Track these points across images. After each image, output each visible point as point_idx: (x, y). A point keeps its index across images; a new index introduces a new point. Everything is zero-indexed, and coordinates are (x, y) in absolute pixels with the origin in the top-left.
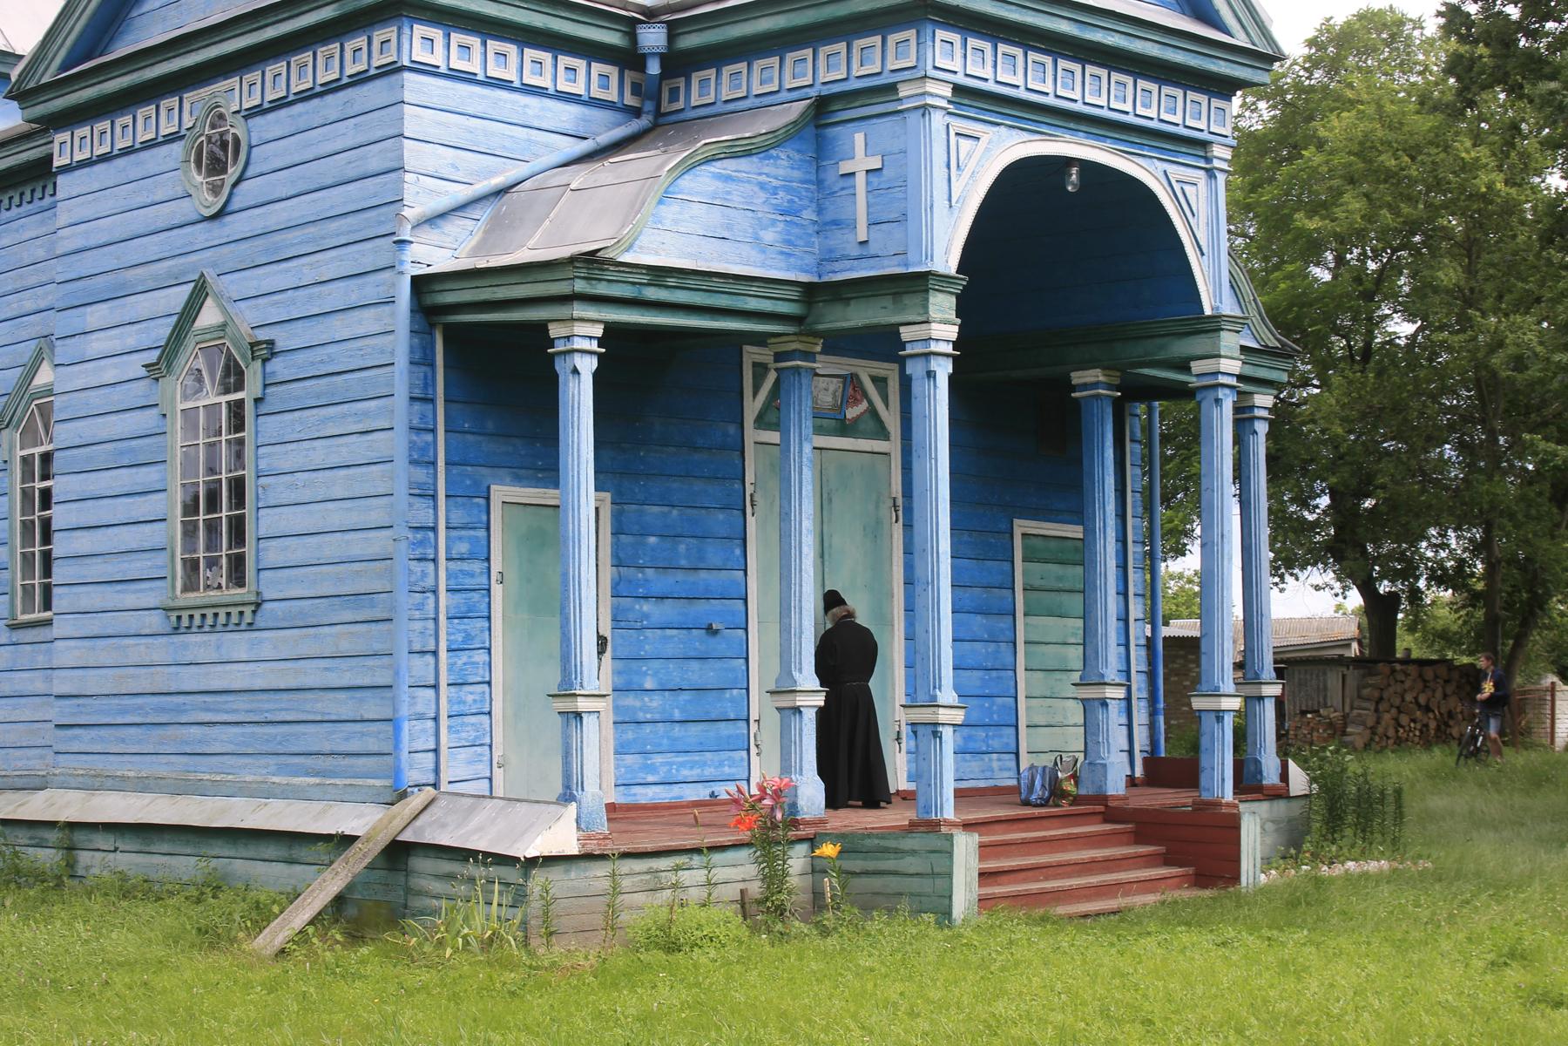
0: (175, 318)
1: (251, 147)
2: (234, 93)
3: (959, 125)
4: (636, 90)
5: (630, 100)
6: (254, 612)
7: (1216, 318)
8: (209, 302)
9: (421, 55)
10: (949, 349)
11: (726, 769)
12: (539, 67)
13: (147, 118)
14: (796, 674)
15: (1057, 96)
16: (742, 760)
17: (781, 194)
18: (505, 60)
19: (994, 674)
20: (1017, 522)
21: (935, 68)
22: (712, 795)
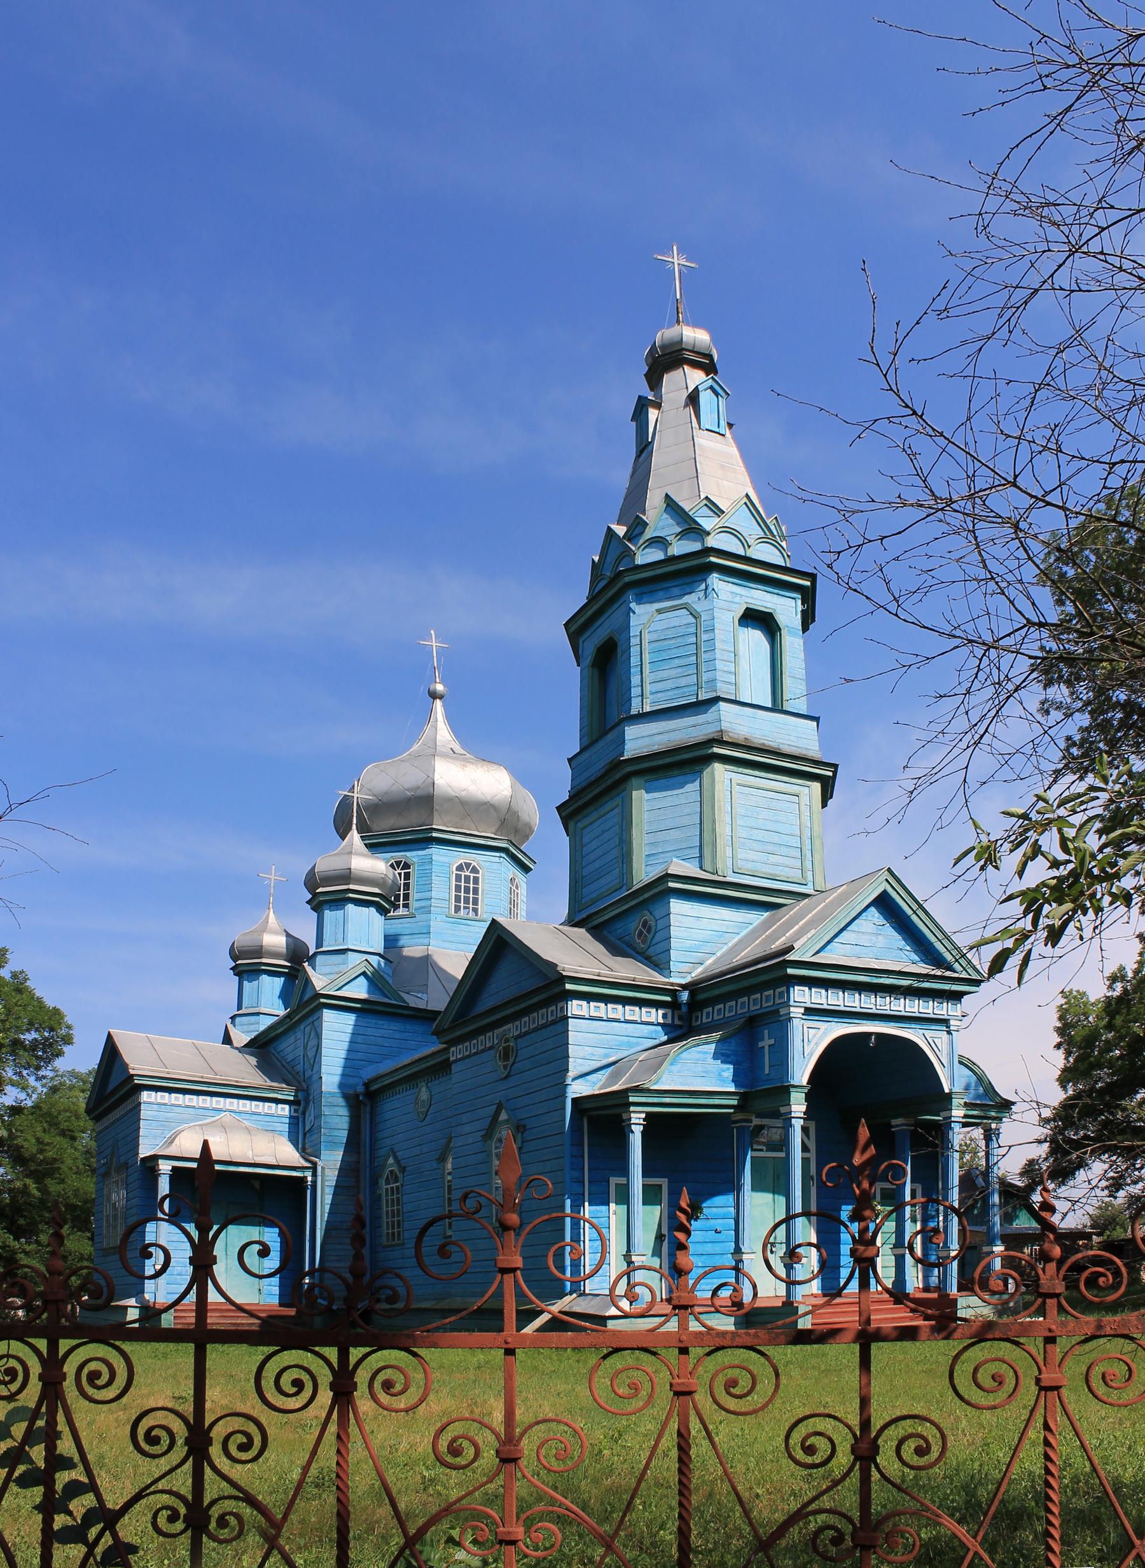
2: (512, 1029)
3: (811, 1024)
4: (680, 1018)
5: (677, 1022)
7: (950, 1094)
8: (503, 1111)
9: (577, 1012)
10: (802, 1115)
12: (633, 1012)
14: (741, 1246)
18: (616, 1011)
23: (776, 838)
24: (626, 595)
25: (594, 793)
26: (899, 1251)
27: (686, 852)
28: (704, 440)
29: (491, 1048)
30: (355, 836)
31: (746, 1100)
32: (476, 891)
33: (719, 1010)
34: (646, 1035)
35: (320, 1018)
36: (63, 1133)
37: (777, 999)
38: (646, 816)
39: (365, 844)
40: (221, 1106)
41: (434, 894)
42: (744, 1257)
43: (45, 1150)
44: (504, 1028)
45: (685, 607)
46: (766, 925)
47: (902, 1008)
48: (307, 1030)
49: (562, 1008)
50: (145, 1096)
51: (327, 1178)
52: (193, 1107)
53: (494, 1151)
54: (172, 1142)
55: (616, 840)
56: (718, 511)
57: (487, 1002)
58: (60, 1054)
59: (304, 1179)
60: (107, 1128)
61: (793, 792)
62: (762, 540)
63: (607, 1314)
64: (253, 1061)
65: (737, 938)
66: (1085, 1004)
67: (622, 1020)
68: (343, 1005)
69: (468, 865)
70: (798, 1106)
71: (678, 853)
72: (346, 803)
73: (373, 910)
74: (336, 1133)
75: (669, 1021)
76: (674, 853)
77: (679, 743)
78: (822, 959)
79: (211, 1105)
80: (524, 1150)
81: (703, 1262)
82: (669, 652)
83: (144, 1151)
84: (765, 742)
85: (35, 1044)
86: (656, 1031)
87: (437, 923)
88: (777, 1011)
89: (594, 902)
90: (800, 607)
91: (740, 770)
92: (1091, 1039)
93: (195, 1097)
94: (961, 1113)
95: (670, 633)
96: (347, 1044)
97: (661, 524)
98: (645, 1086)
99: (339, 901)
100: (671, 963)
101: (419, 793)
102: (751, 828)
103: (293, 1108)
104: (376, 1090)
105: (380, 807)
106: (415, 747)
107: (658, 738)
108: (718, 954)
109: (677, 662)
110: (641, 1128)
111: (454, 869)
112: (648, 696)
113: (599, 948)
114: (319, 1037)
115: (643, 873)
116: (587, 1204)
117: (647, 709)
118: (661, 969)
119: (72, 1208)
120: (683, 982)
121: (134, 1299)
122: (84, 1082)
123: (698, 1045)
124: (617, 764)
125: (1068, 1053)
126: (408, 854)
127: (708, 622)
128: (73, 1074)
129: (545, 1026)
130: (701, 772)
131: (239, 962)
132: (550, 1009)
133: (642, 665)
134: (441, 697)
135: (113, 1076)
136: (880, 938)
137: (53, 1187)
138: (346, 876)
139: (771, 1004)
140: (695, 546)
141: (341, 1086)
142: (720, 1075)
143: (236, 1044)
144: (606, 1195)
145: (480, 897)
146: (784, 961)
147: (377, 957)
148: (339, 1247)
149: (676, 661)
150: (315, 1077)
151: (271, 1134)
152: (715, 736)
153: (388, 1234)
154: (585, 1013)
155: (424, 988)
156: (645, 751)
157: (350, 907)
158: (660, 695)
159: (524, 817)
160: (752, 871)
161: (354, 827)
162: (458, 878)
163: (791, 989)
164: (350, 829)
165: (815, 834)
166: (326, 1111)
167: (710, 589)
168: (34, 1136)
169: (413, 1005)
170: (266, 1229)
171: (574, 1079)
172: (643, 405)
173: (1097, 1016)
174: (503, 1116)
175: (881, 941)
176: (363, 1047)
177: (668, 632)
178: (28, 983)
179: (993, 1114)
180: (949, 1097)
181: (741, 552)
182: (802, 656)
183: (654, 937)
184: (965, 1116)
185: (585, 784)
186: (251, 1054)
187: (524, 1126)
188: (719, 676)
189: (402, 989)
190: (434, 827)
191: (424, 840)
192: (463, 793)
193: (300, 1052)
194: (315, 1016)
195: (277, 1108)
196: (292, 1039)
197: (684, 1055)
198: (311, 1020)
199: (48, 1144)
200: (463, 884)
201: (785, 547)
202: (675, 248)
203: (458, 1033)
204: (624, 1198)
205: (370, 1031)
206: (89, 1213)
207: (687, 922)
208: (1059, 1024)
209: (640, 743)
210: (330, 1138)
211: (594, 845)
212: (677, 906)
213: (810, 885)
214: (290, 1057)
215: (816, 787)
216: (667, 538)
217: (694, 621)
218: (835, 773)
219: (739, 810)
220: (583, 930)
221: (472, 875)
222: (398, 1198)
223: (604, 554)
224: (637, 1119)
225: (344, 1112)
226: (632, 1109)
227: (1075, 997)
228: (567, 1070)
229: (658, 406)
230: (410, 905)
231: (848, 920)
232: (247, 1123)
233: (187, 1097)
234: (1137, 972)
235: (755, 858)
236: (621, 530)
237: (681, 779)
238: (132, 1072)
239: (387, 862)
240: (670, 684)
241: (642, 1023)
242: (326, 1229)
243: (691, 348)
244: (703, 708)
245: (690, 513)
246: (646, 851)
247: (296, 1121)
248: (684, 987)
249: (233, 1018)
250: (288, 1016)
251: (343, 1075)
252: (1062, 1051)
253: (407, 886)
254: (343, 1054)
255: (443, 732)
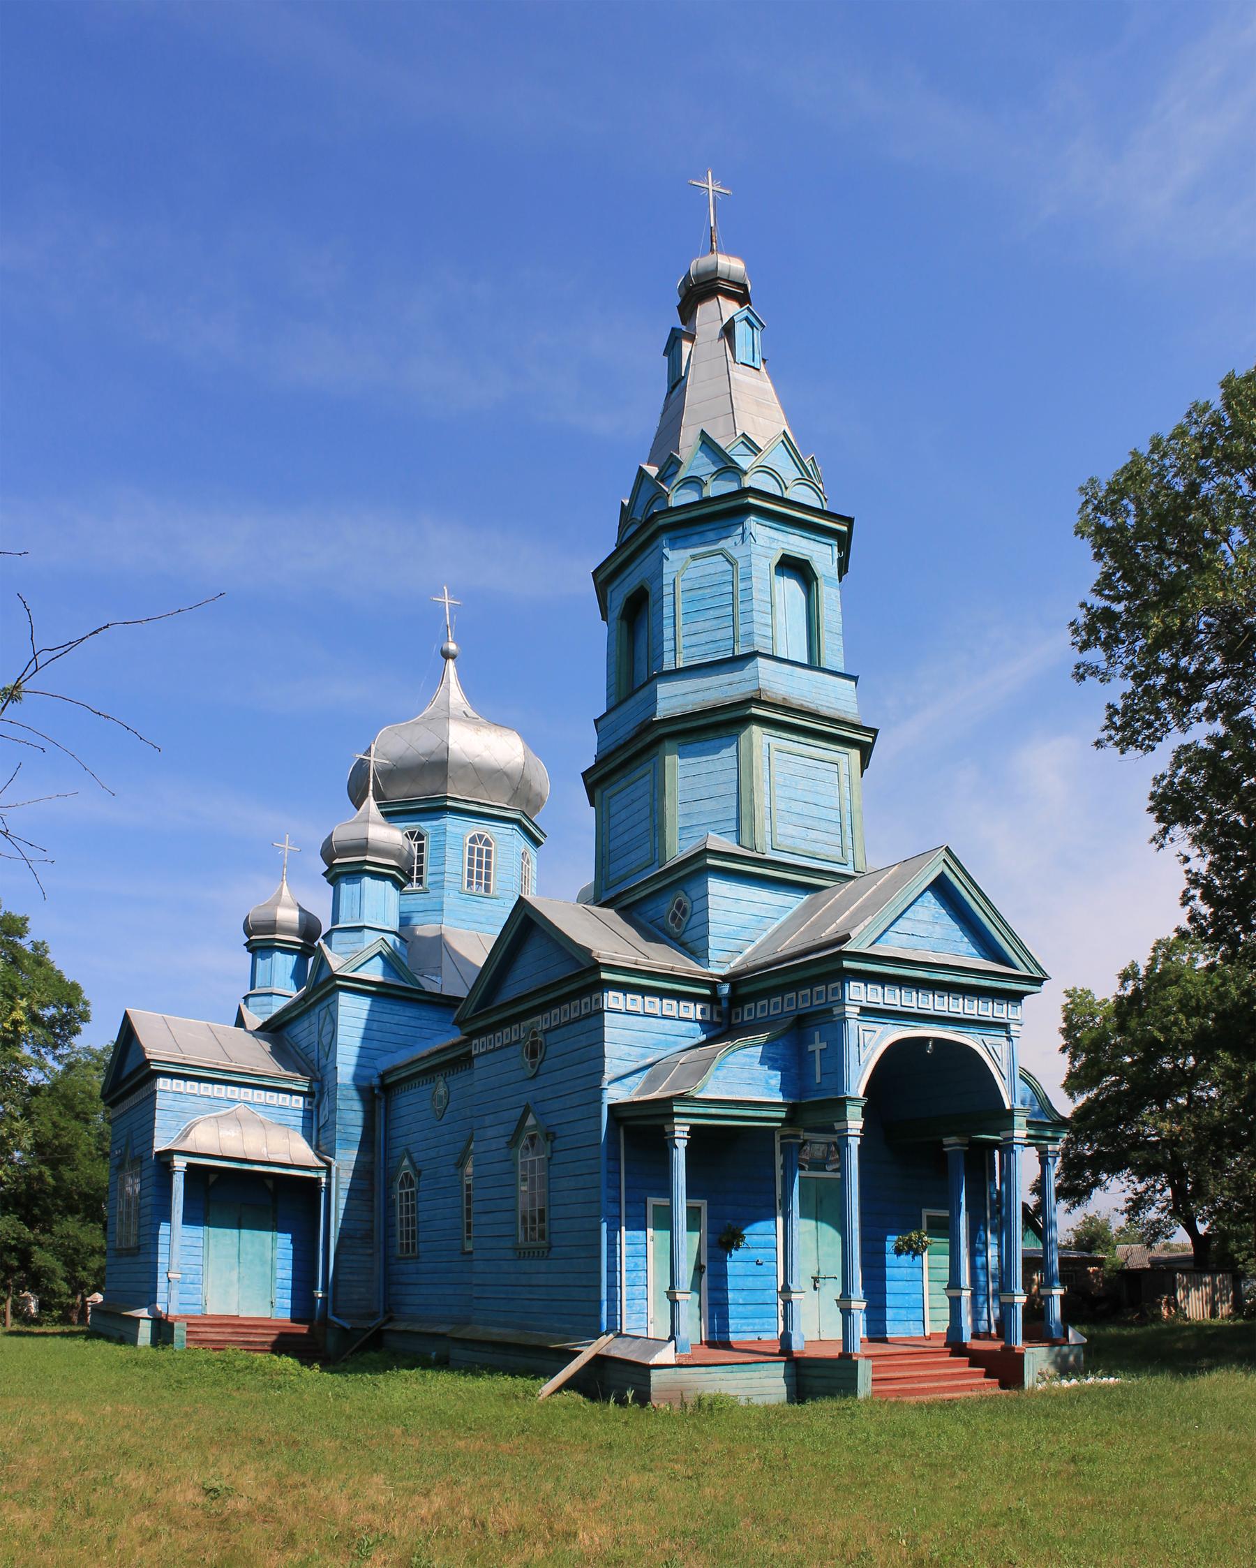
0: (517, 1122)
1: (546, 1047)
2: (541, 1022)
4: (720, 1014)
5: (716, 1019)
6: (548, 1252)
8: (531, 1114)
9: (613, 1005)
10: (858, 1133)
11: (766, 1327)
13: (516, 1030)
14: (790, 1284)
15: (918, 1008)
16: (774, 1322)
17: (780, 1062)
18: (653, 1004)
19: (911, 1283)
20: (923, 1210)
21: (850, 1000)
22: (759, 1339)
23: (815, 811)
24: (659, 540)
25: (623, 758)
26: (954, 1293)
27: (723, 825)
28: (740, 375)
29: (517, 1042)
30: (371, 804)
31: (796, 1113)
32: (488, 865)
33: (763, 1007)
34: (681, 1033)
35: (336, 1002)
36: (77, 1117)
37: (829, 996)
38: (680, 783)
39: (382, 813)
40: (235, 1097)
41: (447, 868)
42: (794, 1296)
43: (60, 1135)
44: (532, 1020)
45: (721, 553)
46: (808, 910)
47: (960, 1010)
48: (323, 1014)
49: (597, 1000)
50: (161, 1083)
51: (341, 1180)
52: (208, 1097)
53: (520, 1161)
54: (187, 1136)
55: (646, 811)
56: (754, 449)
57: (511, 991)
58: (76, 1032)
59: (317, 1180)
60: (121, 1116)
61: (832, 760)
62: (800, 482)
63: (651, 1363)
64: (267, 1046)
65: (777, 924)
66: (1091, 1003)
67: (660, 1015)
68: (359, 988)
69: (481, 837)
70: (855, 1123)
71: (714, 826)
72: (361, 767)
73: (389, 884)
74: (351, 1130)
75: (708, 1017)
76: (709, 826)
77: (715, 702)
78: (880, 950)
79: (226, 1095)
80: (553, 1162)
81: (744, 1299)
82: (704, 602)
83: (159, 1145)
84: (804, 703)
85: (53, 1021)
86: (694, 1029)
87: (450, 899)
88: (830, 1011)
89: (623, 879)
90: (836, 555)
91: (778, 734)
92: (1097, 1045)
93: (210, 1086)
94: (1023, 1133)
95: (704, 582)
96: (362, 1031)
97: (695, 463)
98: (690, 1094)
99: (355, 873)
100: (710, 951)
101: (434, 758)
102: (790, 799)
103: (307, 1099)
104: (392, 1083)
105: (391, 774)
106: (428, 711)
107: (691, 697)
108: (757, 942)
109: (712, 613)
110: (685, 1142)
111: (468, 841)
112: (682, 650)
113: (630, 932)
114: (334, 1022)
115: (678, 848)
116: (623, 1228)
117: (681, 664)
118: (698, 958)
119: (85, 1196)
120: (723, 972)
121: (146, 1310)
122: (99, 1060)
123: (745, 1047)
124: (649, 725)
125: (1074, 1057)
126: (422, 824)
127: (745, 570)
128: (88, 1051)
129: (577, 1020)
130: (738, 735)
131: (253, 937)
132: (584, 1001)
133: (675, 616)
134: (453, 657)
135: (129, 1060)
136: (937, 927)
137: (68, 1174)
138: (363, 847)
139: (823, 1001)
140: (730, 487)
141: (356, 1077)
142: (767, 1083)
143: (249, 1028)
144: (643, 1218)
145: (492, 872)
146: (841, 952)
147: (393, 936)
148: (351, 1257)
149: (711, 612)
150: (330, 1067)
151: (285, 1129)
152: (753, 695)
153: (402, 1244)
154: (621, 1006)
155: (438, 970)
156: (678, 712)
157: (367, 880)
158: (694, 649)
159: (536, 786)
160: (791, 847)
161: (371, 793)
162: (471, 851)
163: (847, 985)
164: (367, 795)
165: (855, 807)
166: (341, 1104)
167: (747, 533)
168: (50, 1119)
169: (428, 989)
170: (280, 1235)
171: (610, 1083)
172: (676, 338)
173: (1104, 1018)
174: (531, 1121)
175: (938, 931)
176: (378, 1035)
177: (703, 580)
178: (48, 956)
179: (1049, 1134)
180: (1010, 1114)
181: (778, 493)
182: (839, 609)
183: (690, 919)
184: (1028, 1137)
185: (613, 747)
186: (265, 1039)
187: (554, 1134)
188: (757, 629)
189: (417, 971)
190: (449, 795)
191: (438, 809)
192: (477, 759)
193: (315, 1038)
194: (330, 1000)
195: (291, 1100)
196: (306, 1024)
197: (731, 1059)
198: (325, 1003)
199: (64, 1129)
200: (476, 858)
201: (822, 489)
202: (710, 173)
203: (480, 1024)
204: (665, 1221)
205: (386, 1018)
206: (100, 1201)
207: (727, 905)
208: (1064, 1025)
209: (674, 702)
210: (344, 1136)
211: (623, 815)
212: (716, 886)
213: (851, 865)
214: (304, 1044)
215: (855, 754)
216: (702, 478)
217: (730, 568)
218: (874, 739)
219: (777, 779)
220: (611, 911)
221: (485, 848)
222: (413, 1205)
223: (633, 499)
224: (681, 1131)
225: (357, 1106)
226: (676, 1120)
227: (1080, 997)
228: (603, 1072)
229: (692, 338)
230: (424, 880)
231: (905, 906)
232: (261, 1116)
233: (203, 1085)
234: (1150, 969)
235: (794, 833)
236: (653, 471)
237: (717, 742)
238: (148, 1056)
239: (402, 832)
240: (704, 638)
241: (681, 1019)
242: (340, 1238)
243: (726, 278)
244: (740, 664)
245: (727, 451)
246: (680, 823)
247: (309, 1114)
248: (725, 979)
249: (246, 998)
250: (303, 998)
251: (358, 1066)
252: (1067, 1054)
253: (420, 859)
254: (358, 1042)
255: (455, 694)
